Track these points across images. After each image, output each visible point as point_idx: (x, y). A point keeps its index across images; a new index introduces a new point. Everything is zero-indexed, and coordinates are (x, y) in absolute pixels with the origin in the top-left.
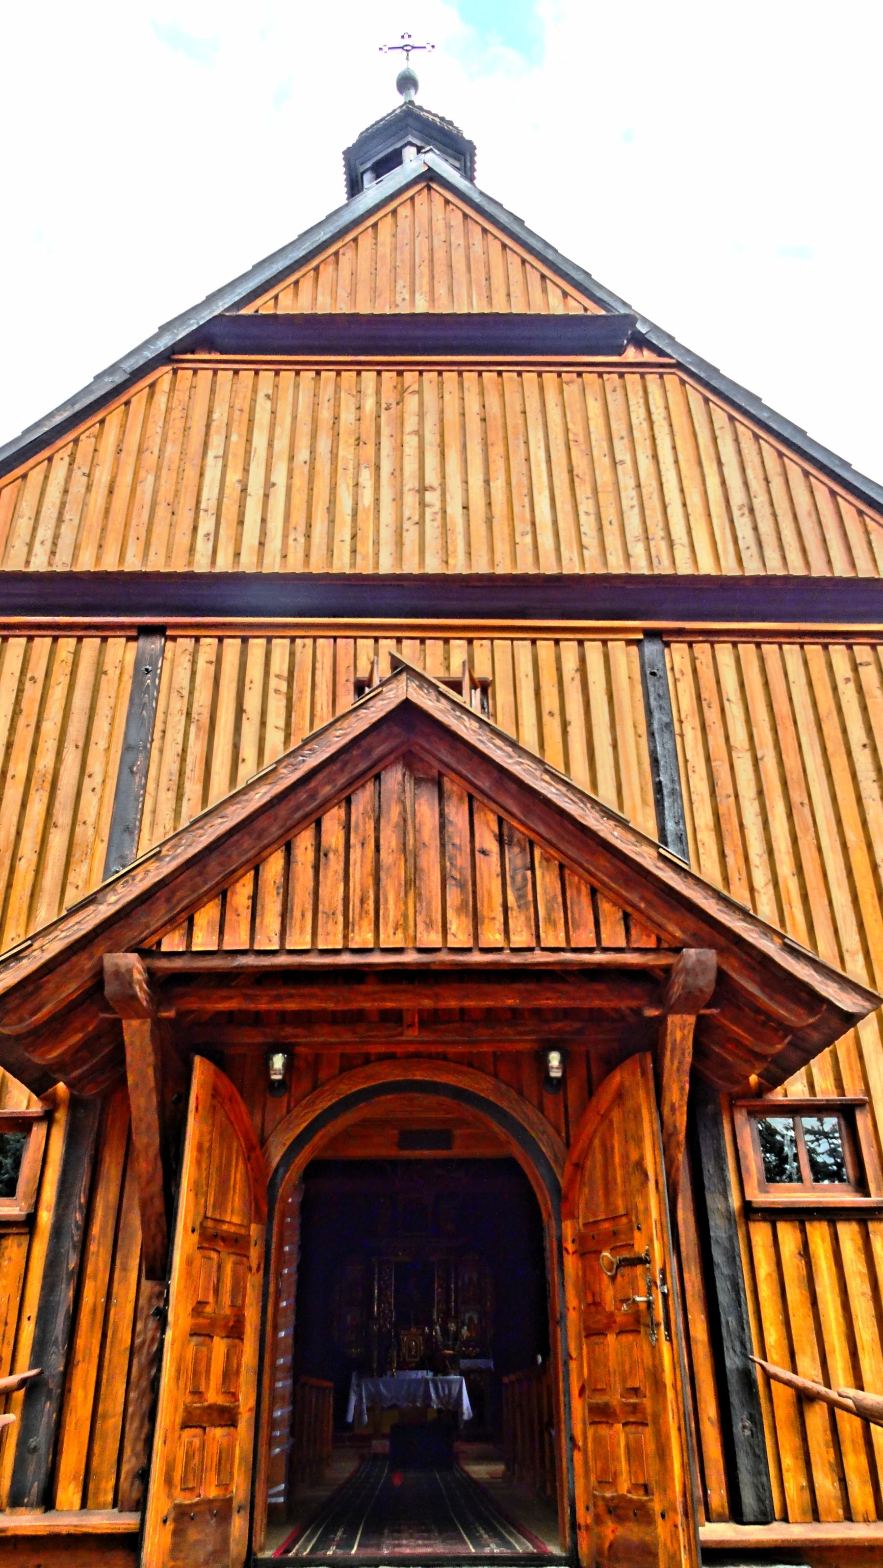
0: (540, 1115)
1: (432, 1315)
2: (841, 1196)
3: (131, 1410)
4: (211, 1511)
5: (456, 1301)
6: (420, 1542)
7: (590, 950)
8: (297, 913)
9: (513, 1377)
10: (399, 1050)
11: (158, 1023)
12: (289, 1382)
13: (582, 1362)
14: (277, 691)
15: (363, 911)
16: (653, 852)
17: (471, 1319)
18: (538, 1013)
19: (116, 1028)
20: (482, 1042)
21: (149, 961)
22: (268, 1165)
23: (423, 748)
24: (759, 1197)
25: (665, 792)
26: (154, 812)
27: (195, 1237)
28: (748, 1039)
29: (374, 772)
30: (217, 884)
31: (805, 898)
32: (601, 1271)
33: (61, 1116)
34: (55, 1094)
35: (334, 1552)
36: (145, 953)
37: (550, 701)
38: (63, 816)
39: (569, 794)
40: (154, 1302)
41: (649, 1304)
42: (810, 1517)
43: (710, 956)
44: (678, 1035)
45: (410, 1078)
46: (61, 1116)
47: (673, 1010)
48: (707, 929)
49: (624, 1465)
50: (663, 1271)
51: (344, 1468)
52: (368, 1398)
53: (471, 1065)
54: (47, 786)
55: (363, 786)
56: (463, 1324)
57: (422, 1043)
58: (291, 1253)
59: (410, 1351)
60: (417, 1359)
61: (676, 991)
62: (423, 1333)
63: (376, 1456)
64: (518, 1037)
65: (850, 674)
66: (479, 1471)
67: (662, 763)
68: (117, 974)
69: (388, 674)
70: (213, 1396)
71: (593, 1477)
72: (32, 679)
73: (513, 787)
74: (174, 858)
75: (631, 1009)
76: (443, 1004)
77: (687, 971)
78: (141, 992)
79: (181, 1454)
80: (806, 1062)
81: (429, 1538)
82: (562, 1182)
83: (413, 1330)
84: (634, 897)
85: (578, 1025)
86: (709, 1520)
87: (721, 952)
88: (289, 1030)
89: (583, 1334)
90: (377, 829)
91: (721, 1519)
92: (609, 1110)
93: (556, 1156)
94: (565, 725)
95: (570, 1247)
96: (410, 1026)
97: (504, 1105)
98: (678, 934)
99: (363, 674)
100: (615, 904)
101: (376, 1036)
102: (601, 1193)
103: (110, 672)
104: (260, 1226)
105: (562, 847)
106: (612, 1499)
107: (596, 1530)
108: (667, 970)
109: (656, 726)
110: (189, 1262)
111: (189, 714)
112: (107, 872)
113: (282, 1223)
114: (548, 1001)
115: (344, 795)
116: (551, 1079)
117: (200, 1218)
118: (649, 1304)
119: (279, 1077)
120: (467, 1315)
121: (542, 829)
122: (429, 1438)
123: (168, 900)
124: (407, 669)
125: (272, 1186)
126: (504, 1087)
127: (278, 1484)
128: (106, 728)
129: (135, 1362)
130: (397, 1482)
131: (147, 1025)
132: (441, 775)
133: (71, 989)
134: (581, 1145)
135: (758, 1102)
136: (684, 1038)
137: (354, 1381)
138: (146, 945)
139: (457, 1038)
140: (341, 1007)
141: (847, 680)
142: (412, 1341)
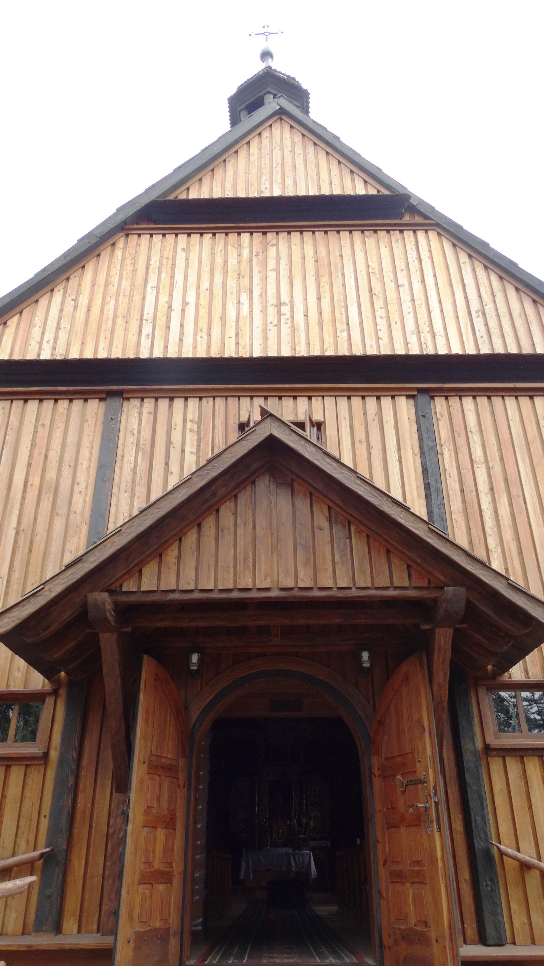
3: (107, 872)
6: (286, 955)
7: (386, 588)
13: (387, 845)
16: (425, 527)
19: (95, 637)
24: (494, 741)
25: (432, 489)
26: (117, 505)
27: (145, 767)
29: (252, 479)
31: (520, 553)
33: (63, 692)
34: (60, 676)
35: (233, 962)
36: (112, 592)
37: (360, 434)
38: (62, 509)
40: (121, 806)
42: (529, 941)
43: (462, 592)
44: (443, 641)
46: (63, 692)
50: (435, 788)
54: (52, 490)
55: (245, 488)
67: (430, 471)
70: (157, 865)
72: (43, 425)
78: (110, 616)
79: (138, 900)
80: (523, 657)
86: (465, 943)
90: (254, 514)
91: (473, 943)
95: (377, 773)
98: (441, 578)
99: (244, 419)
100: (402, 560)
103: (90, 420)
108: (435, 600)
110: (141, 782)
111: (137, 445)
112: (87, 548)
118: (426, 808)
119: (195, 668)
121: (355, 514)
124: (271, 415)
128: (87, 454)
129: (110, 843)
131: (115, 636)
132: (292, 480)
133: (67, 615)
138: (113, 588)
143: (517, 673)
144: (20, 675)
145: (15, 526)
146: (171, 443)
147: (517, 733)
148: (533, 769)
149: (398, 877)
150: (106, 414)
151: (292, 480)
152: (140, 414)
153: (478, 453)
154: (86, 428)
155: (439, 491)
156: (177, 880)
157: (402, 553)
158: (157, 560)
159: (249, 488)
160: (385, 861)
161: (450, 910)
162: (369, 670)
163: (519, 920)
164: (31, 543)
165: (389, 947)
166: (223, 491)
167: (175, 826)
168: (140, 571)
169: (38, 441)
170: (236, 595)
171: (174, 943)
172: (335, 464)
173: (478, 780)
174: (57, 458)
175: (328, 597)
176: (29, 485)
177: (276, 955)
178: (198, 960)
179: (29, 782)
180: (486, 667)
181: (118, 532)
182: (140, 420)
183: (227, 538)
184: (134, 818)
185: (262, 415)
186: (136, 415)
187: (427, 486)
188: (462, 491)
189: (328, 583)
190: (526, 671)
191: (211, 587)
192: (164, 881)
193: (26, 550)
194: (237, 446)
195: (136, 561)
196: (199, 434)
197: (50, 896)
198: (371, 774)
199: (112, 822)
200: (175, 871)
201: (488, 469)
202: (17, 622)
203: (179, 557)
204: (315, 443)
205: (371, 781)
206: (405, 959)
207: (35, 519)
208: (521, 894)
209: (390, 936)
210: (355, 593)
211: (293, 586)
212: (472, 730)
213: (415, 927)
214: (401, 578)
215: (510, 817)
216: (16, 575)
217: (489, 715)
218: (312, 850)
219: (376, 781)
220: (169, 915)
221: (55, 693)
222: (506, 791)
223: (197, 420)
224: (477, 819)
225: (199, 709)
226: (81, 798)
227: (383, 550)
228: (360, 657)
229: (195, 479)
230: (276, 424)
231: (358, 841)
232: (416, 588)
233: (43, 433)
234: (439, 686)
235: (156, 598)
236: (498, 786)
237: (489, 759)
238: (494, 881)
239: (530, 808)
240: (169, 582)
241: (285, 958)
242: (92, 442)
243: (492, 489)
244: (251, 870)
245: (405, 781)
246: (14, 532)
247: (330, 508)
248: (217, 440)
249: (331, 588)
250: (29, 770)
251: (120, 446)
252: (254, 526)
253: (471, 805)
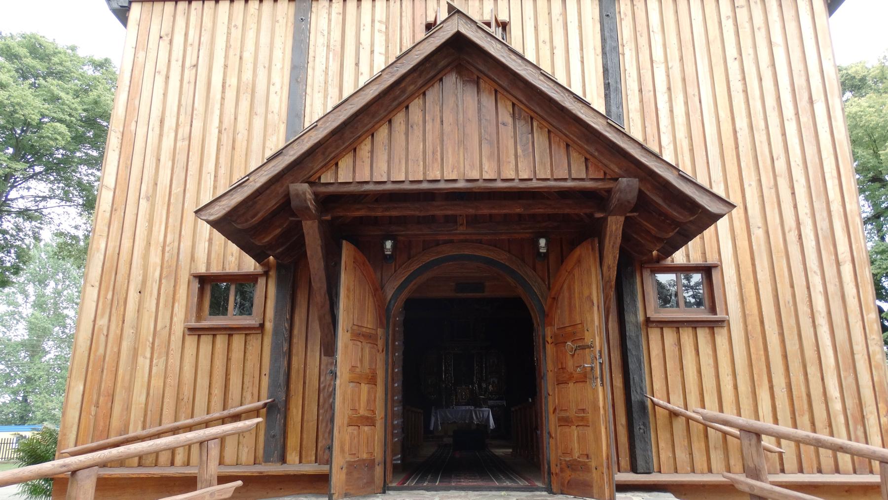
2: (702, 314)
3: (321, 418)
7: (565, 180)
8: (396, 160)
11: (321, 222)
12: (401, 408)
13: (556, 398)
14: (380, 31)
15: (434, 159)
16: (604, 122)
17: (494, 382)
18: (533, 217)
19: (298, 226)
21: (314, 188)
23: (469, 63)
24: (653, 315)
25: (612, 89)
26: (311, 105)
27: (349, 334)
28: (654, 231)
29: (439, 77)
30: (350, 144)
31: (692, 150)
32: (566, 351)
33: (272, 273)
34: (268, 261)
36: (312, 184)
37: (544, 34)
38: (260, 109)
39: (555, 88)
40: (329, 367)
41: (592, 368)
42: (673, 470)
43: (635, 183)
44: (614, 228)
46: (272, 273)
47: (611, 213)
48: (633, 166)
50: (600, 352)
53: (496, 246)
54: (250, 91)
55: (433, 85)
56: (489, 383)
57: (467, 234)
61: (614, 202)
65: (730, 14)
66: (500, 452)
67: (610, 71)
68: (297, 195)
69: (447, 16)
70: (362, 412)
72: (235, 26)
73: (521, 85)
74: (325, 129)
75: (586, 214)
76: (480, 212)
77: (620, 191)
78: (311, 204)
79: (347, 438)
80: (686, 243)
82: (546, 309)
84: (592, 149)
86: (619, 471)
87: (641, 180)
90: (441, 111)
91: (626, 471)
92: (573, 269)
94: (552, 49)
96: (461, 225)
97: (514, 267)
98: (617, 170)
99: (431, 19)
100: (580, 153)
103: (280, 21)
105: (550, 120)
108: (609, 191)
109: (608, 48)
110: (346, 347)
111: (328, 46)
112: (287, 140)
113: (394, 330)
114: (540, 210)
115: (422, 91)
116: (539, 254)
117: (351, 325)
118: (592, 368)
121: (538, 110)
123: (323, 154)
124: (458, 12)
125: (388, 310)
128: (281, 55)
129: (321, 395)
131: (316, 224)
132: (478, 78)
133: (272, 203)
135: (657, 265)
136: (616, 229)
137: (433, 410)
138: (312, 179)
140: (422, 214)
141: (728, 17)
143: (679, 257)
144: (233, 259)
145: (217, 125)
146: (360, 43)
147: (675, 309)
148: (687, 338)
149: (565, 422)
150: (295, 15)
151: (478, 78)
152: (329, 14)
153: (658, 55)
154: (277, 29)
155: (618, 91)
156: (379, 424)
157: (581, 147)
158: (351, 154)
159: (436, 86)
160: (555, 410)
161: (608, 446)
162: (546, 255)
163: (665, 455)
164: (234, 141)
166: (412, 88)
168: (337, 164)
169: (232, 42)
170: (425, 186)
171: (379, 471)
172: (520, 61)
173: (638, 346)
174: (252, 60)
175: (510, 188)
176: (227, 86)
179: (249, 348)
180: (651, 252)
181: (314, 127)
182: (330, 20)
183: (417, 133)
184: (341, 375)
185: (449, 12)
186: (326, 16)
187: (607, 86)
188: (641, 91)
189: (511, 174)
190: (688, 256)
191: (403, 179)
193: (230, 148)
194: (425, 43)
195: (332, 155)
196: (387, 35)
197: (274, 436)
198: (545, 342)
199: (322, 379)
201: (668, 69)
202: (227, 209)
203: (372, 152)
204: (500, 39)
205: (544, 348)
207: (236, 119)
208: (669, 436)
210: (535, 184)
211: (478, 178)
212: (635, 306)
214: (579, 170)
215: (663, 376)
216: (222, 171)
217: (651, 293)
218: (491, 407)
219: (549, 347)
221: (266, 274)
222: (661, 355)
223: (384, 20)
224: (634, 377)
226: (294, 360)
227: (563, 145)
228: (538, 243)
229: (385, 76)
230: (462, 21)
231: (530, 400)
232: (592, 179)
233: (236, 34)
234: (609, 267)
235: (352, 188)
236: (655, 351)
237: (649, 329)
238: (646, 425)
239: (682, 369)
240: (363, 175)
242: (284, 43)
243: (669, 89)
246: (217, 131)
247: (514, 105)
248: (404, 41)
249: (513, 180)
250: (249, 338)
251: (311, 46)
252: (442, 122)
253: (630, 366)
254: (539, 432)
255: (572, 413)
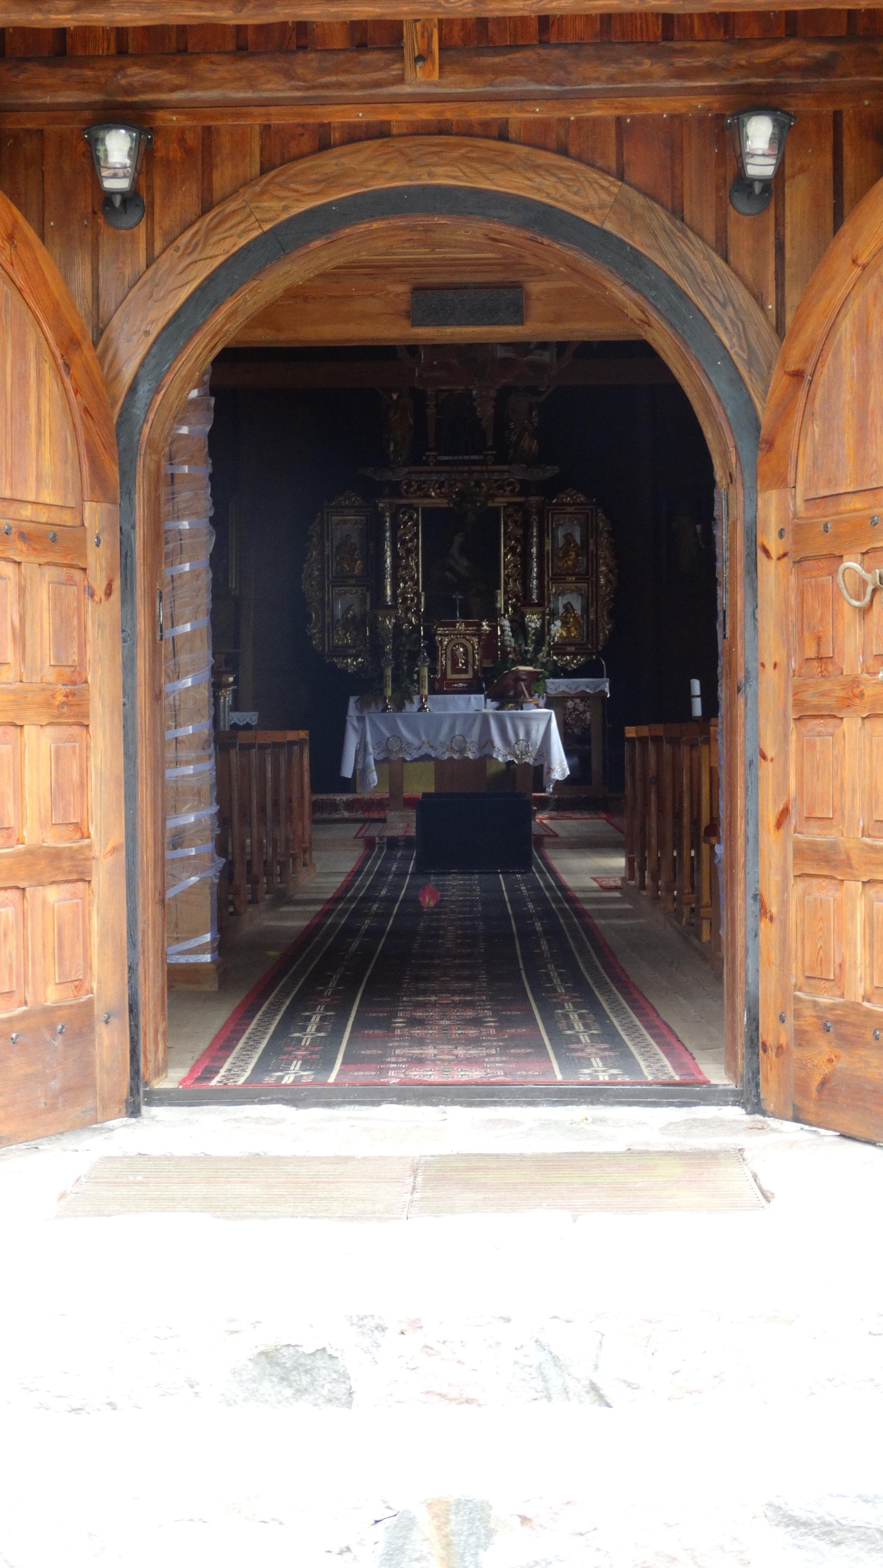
0: (719, 261)
1: (495, 600)
4: (51, 1027)
5: (540, 577)
6: (460, 1052)
9: (645, 731)
10: (396, 117)
12: (208, 766)
17: (568, 608)
20: (589, 95)
22: (111, 380)
35: (298, 1079)
45: (426, 181)
49: (860, 952)
51: (331, 867)
52: (377, 744)
53: (563, 151)
56: (554, 614)
58: (194, 533)
59: (455, 662)
60: (470, 675)
62: (478, 634)
63: (393, 843)
64: (675, 84)
70: (34, 834)
71: (795, 968)
81: (475, 1042)
82: (765, 417)
83: (460, 627)
85: (819, 51)
88: (136, 73)
89: (792, 715)
93: (751, 351)
95: (772, 542)
97: (638, 241)
101: (342, 85)
102: (849, 439)
104: (104, 507)
106: (832, 1008)
107: (796, 1053)
119: (122, 184)
120: (562, 602)
122: (483, 816)
126: (639, 200)
127: (196, 933)
130: (428, 901)
134: (812, 329)
139: (532, 87)
142: (458, 642)
160: (785, 813)
162: (772, 189)
165: (780, 1047)
167: (86, 716)
177: (431, 1051)
178: (192, 1071)
192: (60, 878)
198: (754, 549)
200: (96, 847)
206: (823, 1083)
209: (782, 1020)
213: (866, 1004)
219: (770, 572)
220: (88, 966)
225: (147, 333)
241: (458, 1061)
244: (371, 760)
245: (872, 579)
254: (719, 849)
255: (849, 837)
